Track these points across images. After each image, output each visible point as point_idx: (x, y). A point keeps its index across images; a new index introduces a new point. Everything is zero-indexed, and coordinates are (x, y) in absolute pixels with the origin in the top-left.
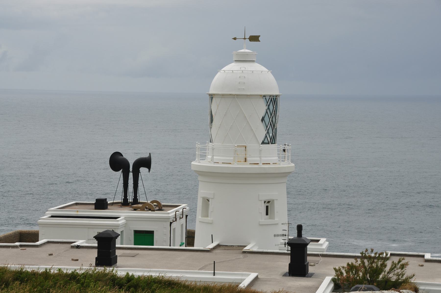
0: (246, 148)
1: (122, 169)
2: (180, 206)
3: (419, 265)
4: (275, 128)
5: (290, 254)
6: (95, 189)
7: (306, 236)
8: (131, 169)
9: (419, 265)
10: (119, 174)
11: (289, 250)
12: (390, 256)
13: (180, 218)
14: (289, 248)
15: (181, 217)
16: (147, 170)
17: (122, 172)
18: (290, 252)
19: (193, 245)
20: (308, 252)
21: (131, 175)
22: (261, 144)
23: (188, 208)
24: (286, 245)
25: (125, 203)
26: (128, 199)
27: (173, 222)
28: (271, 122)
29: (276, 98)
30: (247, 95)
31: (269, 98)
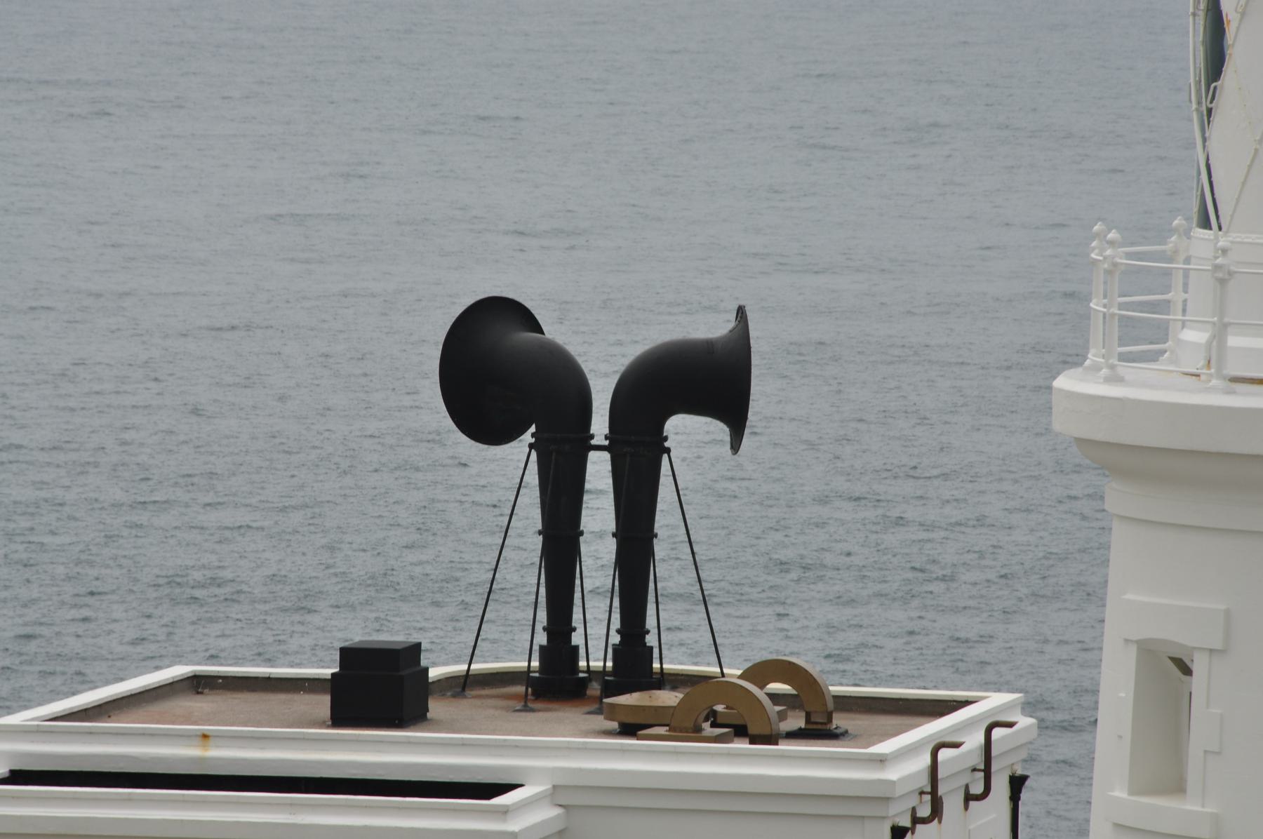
1: (533, 429)
8: (600, 426)
13: (969, 798)
15: (978, 789)
16: (718, 429)
17: (531, 446)
21: (599, 469)
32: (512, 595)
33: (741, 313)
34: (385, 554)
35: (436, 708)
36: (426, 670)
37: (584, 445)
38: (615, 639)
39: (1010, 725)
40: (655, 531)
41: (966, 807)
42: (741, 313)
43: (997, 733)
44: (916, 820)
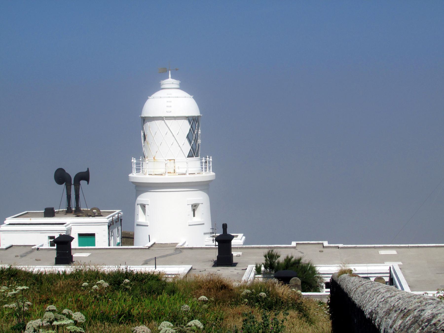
0: (174, 161)
1: (65, 183)
2: (115, 211)
3: (320, 251)
4: (198, 143)
5: (56, 249)
6: (369, 286)
7: (229, 232)
8: (73, 182)
9: (320, 251)
10: (63, 186)
11: (216, 244)
12: (296, 246)
13: (116, 222)
14: (217, 243)
15: (117, 221)
16: (86, 182)
17: (65, 185)
18: (217, 247)
19: (95, 245)
20: (232, 246)
21: (73, 187)
22: (187, 157)
23: (122, 213)
24: (214, 241)
25: (69, 211)
26: (71, 207)
27: (110, 226)
28: (194, 134)
29: (198, 119)
30: (174, 117)
31: (192, 119)
32: (208, 316)
33: (88, 168)
34: (280, 309)
35: (56, 215)
36: (54, 211)
37: (71, 184)
38: (75, 206)
39: (120, 214)
40: (59, 236)
41: (116, 223)
42: (88, 168)
43: (119, 215)
44: (111, 225)
